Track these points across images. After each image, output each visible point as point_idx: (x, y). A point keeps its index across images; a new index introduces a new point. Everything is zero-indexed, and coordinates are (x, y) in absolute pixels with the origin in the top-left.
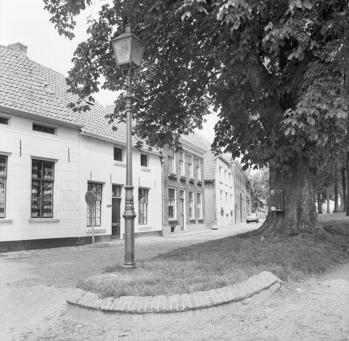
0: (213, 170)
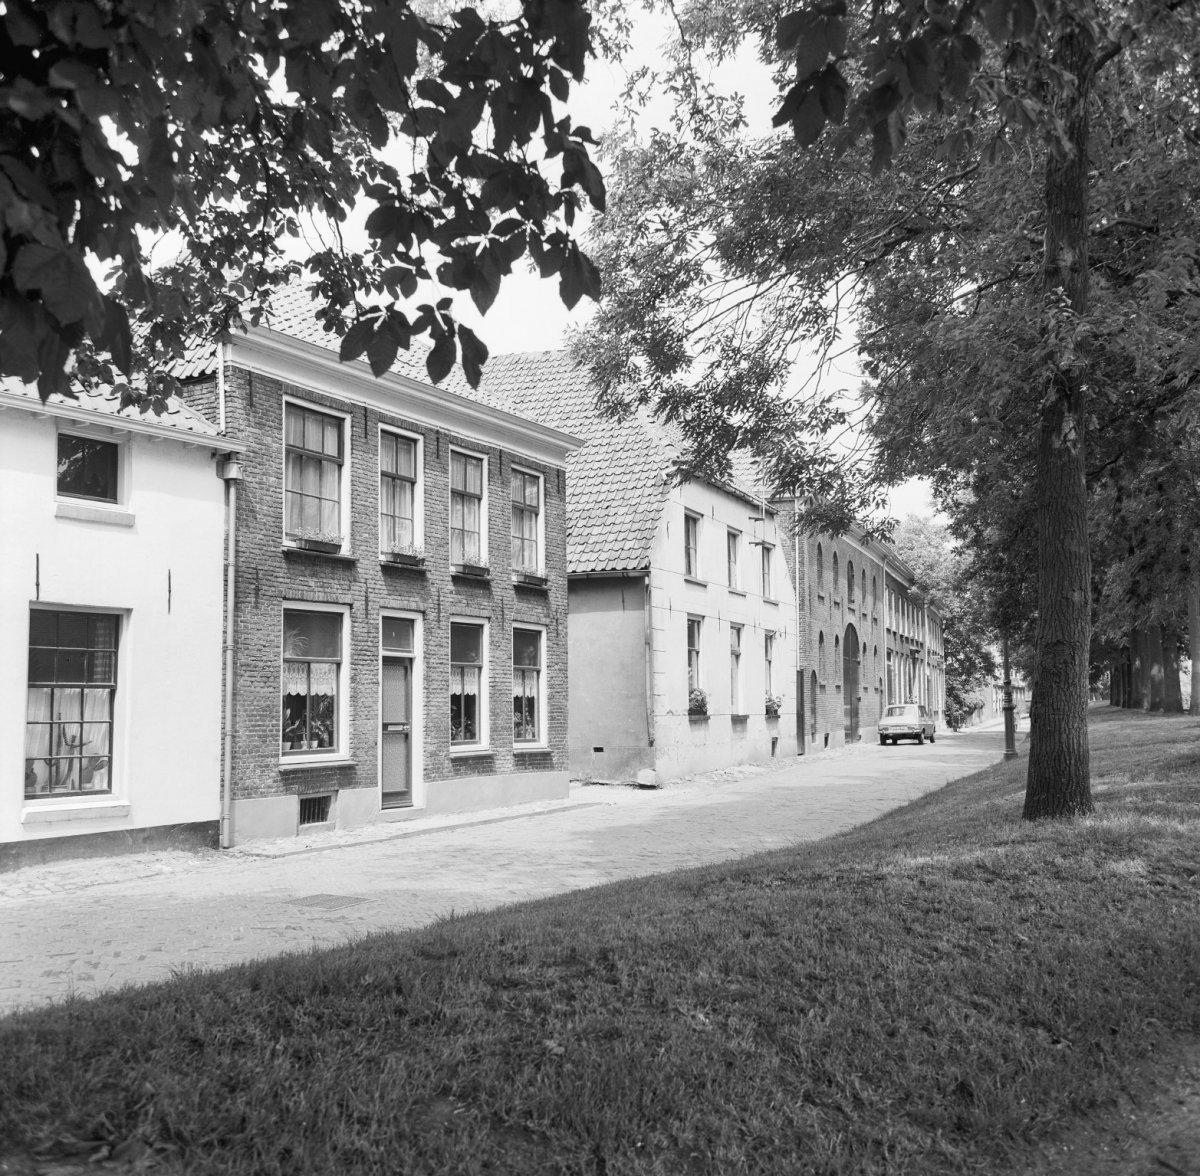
0: (649, 525)
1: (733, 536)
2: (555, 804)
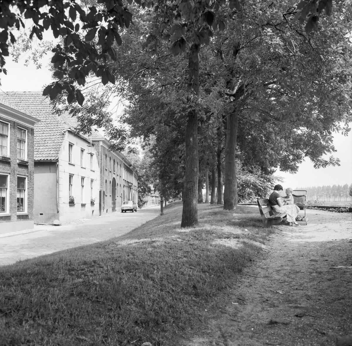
0: (58, 146)
1: (82, 151)
2: (30, 230)
